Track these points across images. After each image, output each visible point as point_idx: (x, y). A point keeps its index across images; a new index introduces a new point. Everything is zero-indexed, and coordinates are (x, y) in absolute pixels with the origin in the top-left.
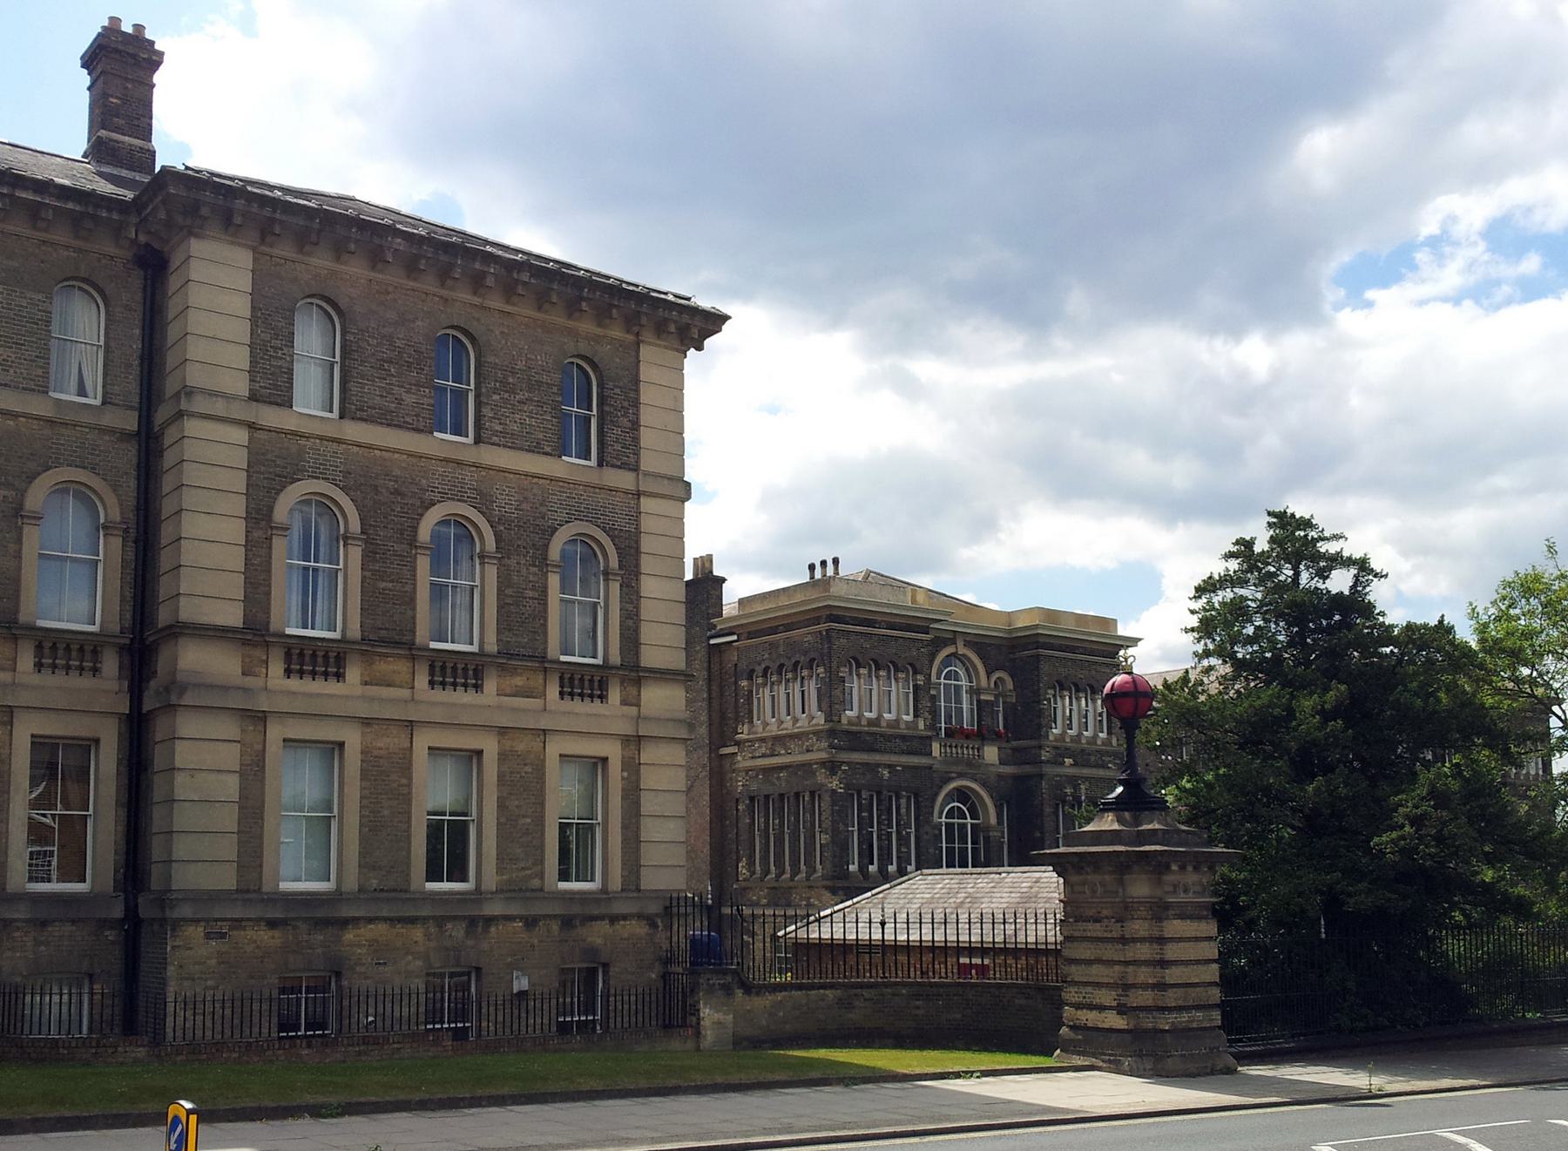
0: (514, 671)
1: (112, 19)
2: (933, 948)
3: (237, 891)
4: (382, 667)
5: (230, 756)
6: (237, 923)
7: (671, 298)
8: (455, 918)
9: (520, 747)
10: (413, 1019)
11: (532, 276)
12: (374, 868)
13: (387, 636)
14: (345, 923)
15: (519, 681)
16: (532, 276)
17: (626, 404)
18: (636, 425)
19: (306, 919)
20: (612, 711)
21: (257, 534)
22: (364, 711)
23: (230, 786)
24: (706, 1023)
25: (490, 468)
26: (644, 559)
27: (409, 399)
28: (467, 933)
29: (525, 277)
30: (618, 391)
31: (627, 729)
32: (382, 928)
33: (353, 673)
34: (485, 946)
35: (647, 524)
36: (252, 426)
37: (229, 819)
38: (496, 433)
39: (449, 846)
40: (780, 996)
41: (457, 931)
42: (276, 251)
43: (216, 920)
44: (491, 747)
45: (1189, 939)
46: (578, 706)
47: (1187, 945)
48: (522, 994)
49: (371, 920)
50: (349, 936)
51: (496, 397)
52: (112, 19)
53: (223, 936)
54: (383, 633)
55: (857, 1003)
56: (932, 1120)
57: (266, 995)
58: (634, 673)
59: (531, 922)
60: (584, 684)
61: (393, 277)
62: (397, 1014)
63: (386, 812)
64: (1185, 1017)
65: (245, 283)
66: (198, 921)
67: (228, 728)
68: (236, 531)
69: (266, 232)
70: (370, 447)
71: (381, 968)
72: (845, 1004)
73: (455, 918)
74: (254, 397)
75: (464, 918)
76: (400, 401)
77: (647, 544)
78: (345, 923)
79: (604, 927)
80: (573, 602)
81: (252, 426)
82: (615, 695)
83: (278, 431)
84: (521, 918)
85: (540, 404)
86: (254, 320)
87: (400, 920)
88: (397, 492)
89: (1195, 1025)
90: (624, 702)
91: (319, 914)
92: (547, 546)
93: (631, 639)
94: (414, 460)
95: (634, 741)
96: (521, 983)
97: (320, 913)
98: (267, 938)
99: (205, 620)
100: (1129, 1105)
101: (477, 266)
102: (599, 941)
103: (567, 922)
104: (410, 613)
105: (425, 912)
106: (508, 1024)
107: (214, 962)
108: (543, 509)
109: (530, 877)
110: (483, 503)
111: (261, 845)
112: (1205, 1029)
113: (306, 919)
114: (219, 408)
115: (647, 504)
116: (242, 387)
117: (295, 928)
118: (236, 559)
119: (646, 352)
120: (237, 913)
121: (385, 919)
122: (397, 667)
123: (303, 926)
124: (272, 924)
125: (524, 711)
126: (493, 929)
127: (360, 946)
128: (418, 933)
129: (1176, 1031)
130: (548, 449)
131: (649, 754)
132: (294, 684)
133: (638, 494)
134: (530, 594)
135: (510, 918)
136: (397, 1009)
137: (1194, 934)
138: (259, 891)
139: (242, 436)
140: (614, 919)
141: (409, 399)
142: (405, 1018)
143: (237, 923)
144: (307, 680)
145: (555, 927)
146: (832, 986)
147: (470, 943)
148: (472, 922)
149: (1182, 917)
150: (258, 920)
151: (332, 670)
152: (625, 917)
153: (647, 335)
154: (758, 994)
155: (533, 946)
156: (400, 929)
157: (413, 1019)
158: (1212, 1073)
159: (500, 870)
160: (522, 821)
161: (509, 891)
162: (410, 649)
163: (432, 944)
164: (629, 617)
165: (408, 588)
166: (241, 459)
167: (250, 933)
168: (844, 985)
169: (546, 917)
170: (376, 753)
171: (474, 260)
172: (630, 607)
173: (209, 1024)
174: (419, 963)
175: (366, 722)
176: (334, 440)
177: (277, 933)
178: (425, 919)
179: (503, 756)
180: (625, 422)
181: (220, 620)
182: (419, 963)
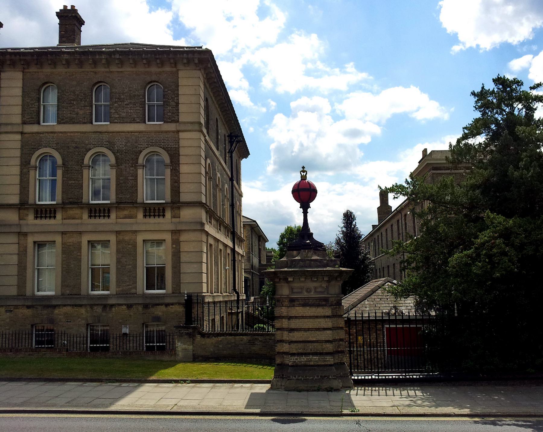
0: (124, 209)
1: (64, 6)
3: (18, 295)
4: (71, 212)
5: (14, 249)
6: (16, 307)
7: (10, 50)
8: (97, 305)
9: (127, 238)
10: (82, 342)
11: (120, 55)
12: (67, 286)
13: (72, 201)
14: (55, 307)
15: (126, 212)
16: (120, 55)
17: (173, 96)
18: (177, 104)
19: (40, 305)
20: (167, 221)
21: (25, 170)
22: (117, 228)
23: (15, 259)
24: (179, 349)
26: (181, 158)
27: (81, 112)
28: (103, 311)
29: (117, 56)
30: (170, 92)
31: (172, 227)
32: (68, 309)
33: (59, 216)
34: (111, 315)
35: (182, 143)
36: (22, 133)
37: (14, 270)
38: (116, 118)
39: (155, 277)
40: (220, 338)
41: (99, 310)
42: (30, 70)
43: (9, 306)
44: (113, 238)
45: (310, 317)
46: (152, 220)
48: (125, 334)
49: (65, 306)
50: (56, 311)
52: (64, 6)
53: (11, 311)
54: (71, 200)
55: (256, 342)
56: (9, 405)
57: (27, 332)
58: (176, 204)
59: (129, 306)
60: (154, 211)
61: (73, 69)
63: (72, 266)
64: (304, 359)
65: (20, 84)
67: (14, 239)
68: (16, 170)
69: (27, 64)
70: (65, 133)
71: (69, 323)
72: (251, 343)
73: (97, 305)
74: (24, 123)
75: (101, 305)
76: (77, 114)
77: (182, 151)
78: (55, 307)
79: (163, 308)
80: (154, 179)
81: (22, 133)
82: (168, 214)
83: (32, 133)
84: (125, 305)
85: (134, 104)
86: (23, 96)
87: (76, 306)
88: (77, 147)
89: (312, 363)
90: (173, 217)
91: (47, 303)
92: (138, 159)
93: (176, 190)
94: (82, 135)
95: (176, 233)
96: (125, 330)
97: (44, 303)
98: (27, 312)
99: (6, 202)
100: (142, 406)
101: (97, 57)
102: (160, 314)
103: (146, 306)
104: (81, 191)
105: (85, 302)
107: (8, 320)
108: (136, 144)
109: (131, 288)
110: (111, 146)
111: (26, 280)
112: (318, 366)
113: (40, 305)
114: (9, 128)
115: (182, 135)
116: (18, 119)
117: (37, 308)
118: (17, 180)
119: (181, 74)
120: (16, 303)
121: (70, 305)
122: (76, 212)
123: (40, 308)
124: (28, 307)
125: (127, 224)
127: (60, 315)
128: (83, 310)
129: (295, 366)
130: (139, 121)
131: (184, 237)
132: (38, 221)
133: (178, 132)
134: (131, 178)
135: (121, 305)
138: (25, 296)
139: (19, 137)
140: (167, 305)
141: (81, 112)
142: (131, 342)
143: (16, 307)
144: (48, 220)
145: (140, 308)
146: (245, 335)
147: (104, 314)
148: (105, 306)
150: (23, 305)
151: (157, 214)
152: (172, 304)
153: (180, 66)
154: (208, 337)
155: (130, 316)
156: (76, 309)
157: (82, 342)
158: (318, 390)
159: (118, 286)
160: (127, 267)
161: (118, 295)
162: (134, 203)
164: (176, 182)
165: (80, 182)
166: (18, 145)
167: (21, 310)
168: (250, 334)
169: (136, 304)
170: (68, 244)
171: (129, 55)
172: (176, 178)
173: (7, 342)
174: (83, 322)
175: (63, 233)
176: (52, 133)
177: (30, 310)
178: (85, 305)
179: (118, 242)
180: (173, 103)
181: (11, 202)
182: (83, 322)
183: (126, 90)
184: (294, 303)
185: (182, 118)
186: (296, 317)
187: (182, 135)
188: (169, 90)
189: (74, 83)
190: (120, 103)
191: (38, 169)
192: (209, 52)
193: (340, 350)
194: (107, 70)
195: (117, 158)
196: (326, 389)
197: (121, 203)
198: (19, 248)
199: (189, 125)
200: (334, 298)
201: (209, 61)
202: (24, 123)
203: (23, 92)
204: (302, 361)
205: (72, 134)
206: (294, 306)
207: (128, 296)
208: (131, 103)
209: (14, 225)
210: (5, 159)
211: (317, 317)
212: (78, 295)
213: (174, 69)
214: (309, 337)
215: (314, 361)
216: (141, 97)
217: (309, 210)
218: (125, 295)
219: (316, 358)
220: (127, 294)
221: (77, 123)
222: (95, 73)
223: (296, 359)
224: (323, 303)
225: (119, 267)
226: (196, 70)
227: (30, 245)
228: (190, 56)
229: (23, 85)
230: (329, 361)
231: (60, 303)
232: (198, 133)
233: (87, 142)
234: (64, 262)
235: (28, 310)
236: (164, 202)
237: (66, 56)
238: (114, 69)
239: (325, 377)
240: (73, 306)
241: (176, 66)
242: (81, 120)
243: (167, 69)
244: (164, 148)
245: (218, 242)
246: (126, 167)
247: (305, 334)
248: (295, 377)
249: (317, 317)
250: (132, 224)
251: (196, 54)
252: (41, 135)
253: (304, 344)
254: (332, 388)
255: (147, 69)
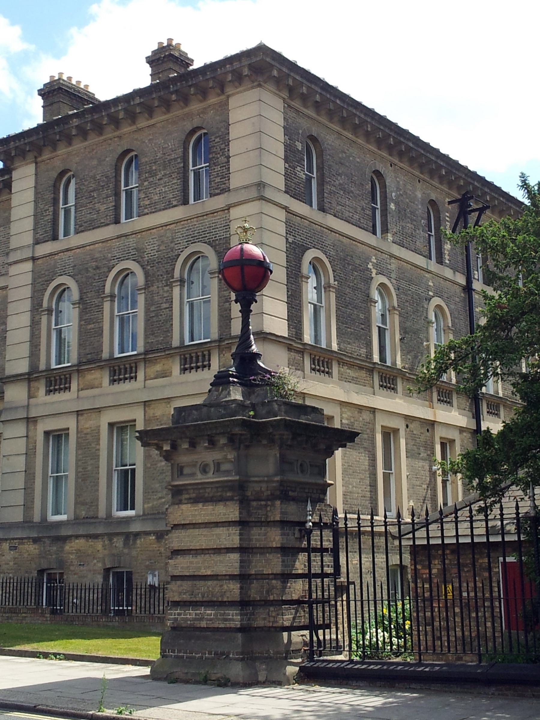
2: (458, 548)
11: (140, 98)
14: (65, 539)
15: (158, 367)
16: (140, 98)
19: (49, 537)
25: (141, 232)
27: (103, 208)
32: (81, 542)
34: (134, 553)
36: (34, 259)
37: (19, 482)
41: (119, 542)
47: (196, 532)
48: (152, 587)
49: (77, 537)
51: (146, 183)
53: (16, 548)
62: (91, 598)
64: (191, 614)
66: (6, 540)
70: (83, 246)
71: (82, 568)
74: (37, 242)
76: (98, 211)
81: (34, 259)
88: (97, 268)
89: (203, 624)
94: (104, 244)
98: (32, 549)
106: (147, 609)
107: (11, 563)
108: (172, 245)
112: (217, 629)
116: (29, 239)
120: (19, 534)
123: (48, 542)
124: (35, 540)
126: (138, 542)
127: (72, 553)
128: (99, 545)
130: (175, 203)
136: (91, 595)
137: (207, 519)
147: (126, 551)
149: (195, 501)
150: (29, 538)
153: (229, 90)
156: (91, 542)
159: (146, 500)
163: (106, 552)
171: (110, 108)
176: (68, 250)
177: (36, 546)
183: (159, 155)
184: (180, 498)
185: (235, 181)
186: (184, 526)
187: (235, 213)
188: (216, 138)
189: (95, 162)
190: (151, 179)
191: (54, 313)
192: (262, 49)
193: (271, 598)
194: (134, 128)
195: (147, 275)
196: (218, 680)
197: (152, 351)
198: (27, 442)
199: (243, 191)
200: (264, 486)
201: (272, 66)
202: (37, 242)
203: (36, 193)
204: (187, 620)
205: (92, 247)
206: (180, 502)
207: (157, 516)
208: (165, 175)
209: (19, 407)
210: (15, 303)
211: (217, 524)
212: (93, 518)
213: (223, 97)
214: (200, 568)
215: (207, 620)
216: (179, 160)
217: (253, 307)
218: (152, 516)
219: (210, 612)
220: (159, 513)
221: (99, 227)
222: (120, 137)
223: (179, 614)
224: (229, 494)
225: (149, 465)
226: (252, 88)
227: (40, 438)
228: (236, 65)
229: (36, 182)
230: (232, 620)
231: (70, 533)
232: (257, 203)
233: (110, 255)
234: (80, 463)
235: (34, 546)
236: (209, 340)
237: (75, 122)
238: (142, 123)
239: (223, 654)
240: (88, 537)
241: (223, 92)
242: (102, 221)
243: (213, 100)
244: (209, 244)
245: (374, 412)
246: (158, 287)
247: (195, 560)
248: (173, 651)
249: (217, 524)
250: (164, 386)
251: (243, 60)
252: (56, 257)
253: (190, 583)
254: (228, 680)
255: (187, 110)
